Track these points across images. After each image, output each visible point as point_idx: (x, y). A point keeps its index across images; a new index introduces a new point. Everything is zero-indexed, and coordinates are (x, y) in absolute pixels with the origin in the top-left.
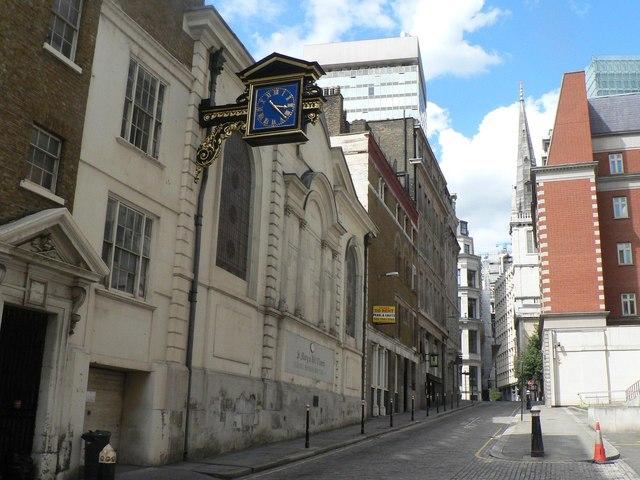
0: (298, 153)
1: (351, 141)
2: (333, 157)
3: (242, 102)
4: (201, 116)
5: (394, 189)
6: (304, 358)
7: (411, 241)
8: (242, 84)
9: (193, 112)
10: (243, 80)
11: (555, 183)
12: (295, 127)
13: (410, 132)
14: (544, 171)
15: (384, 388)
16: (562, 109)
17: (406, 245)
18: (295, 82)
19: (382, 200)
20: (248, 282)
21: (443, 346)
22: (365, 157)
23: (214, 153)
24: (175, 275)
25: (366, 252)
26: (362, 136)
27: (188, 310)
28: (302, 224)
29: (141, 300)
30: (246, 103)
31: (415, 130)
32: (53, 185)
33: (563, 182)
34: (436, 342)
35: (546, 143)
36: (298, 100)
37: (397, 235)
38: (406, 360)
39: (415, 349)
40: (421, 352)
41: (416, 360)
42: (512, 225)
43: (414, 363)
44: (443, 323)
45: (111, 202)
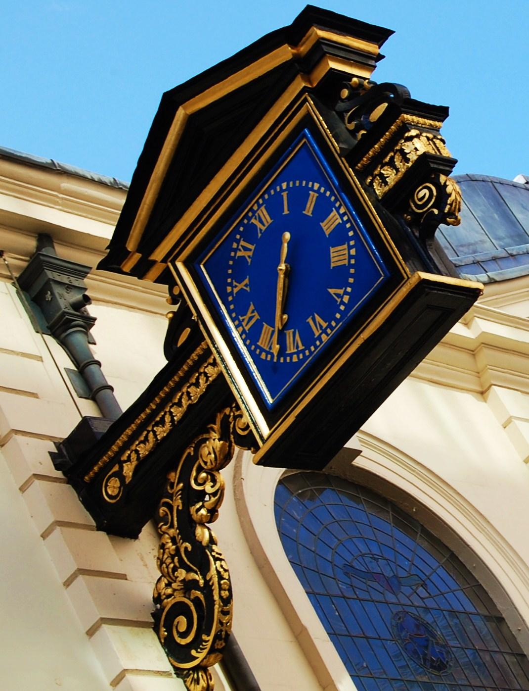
0: (482, 371)
3: (184, 344)
4: (90, 498)
8: (148, 282)
9: (58, 499)
10: (140, 271)
16: (160, 633)
18: (297, 133)
23: (207, 589)
32: (310, 485)
36: (346, 187)
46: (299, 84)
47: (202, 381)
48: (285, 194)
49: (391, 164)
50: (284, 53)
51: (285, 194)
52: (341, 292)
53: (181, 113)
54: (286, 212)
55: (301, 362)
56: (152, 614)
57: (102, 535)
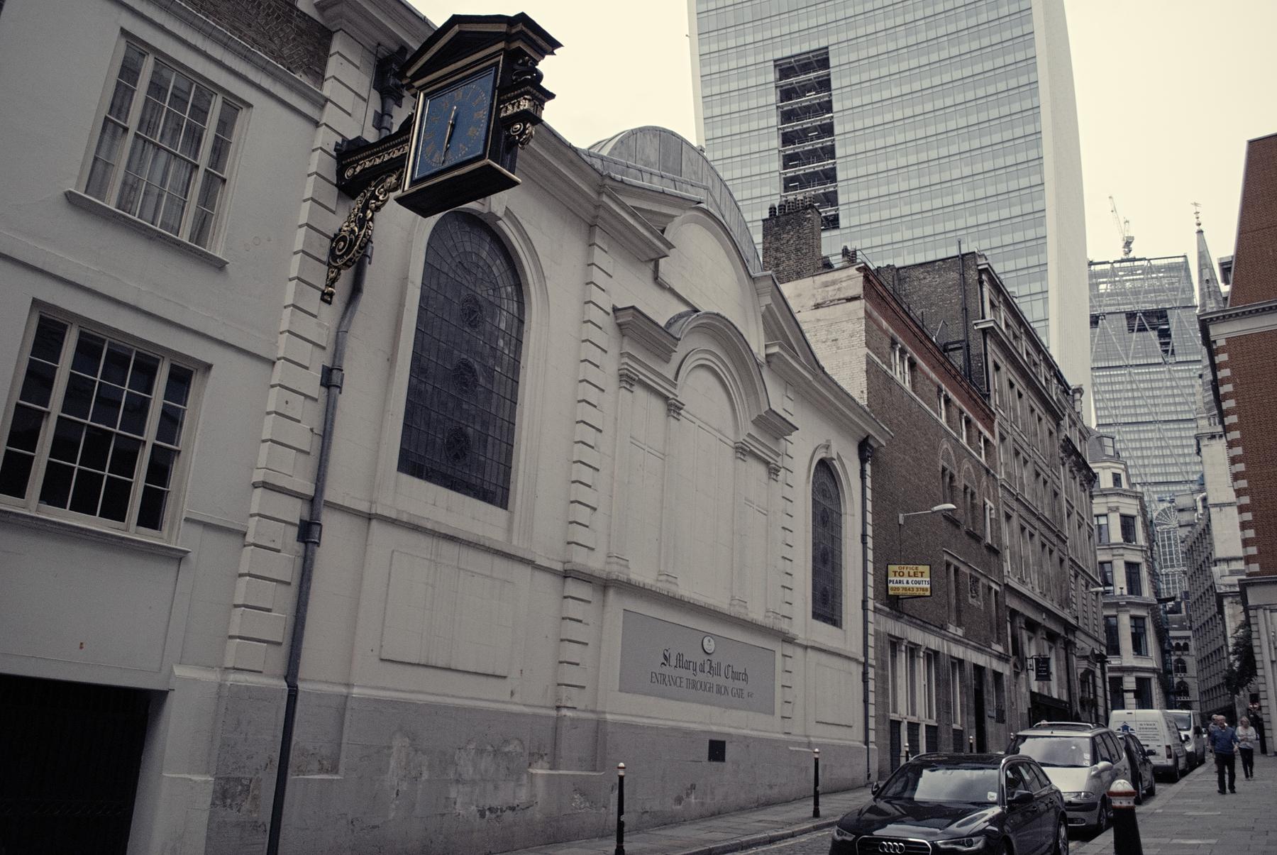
1: (834, 282)
4: (340, 173)
5: (933, 368)
6: (682, 663)
7: (983, 460)
11: (1248, 338)
13: (972, 276)
14: (1225, 318)
15: (924, 717)
17: (966, 465)
19: (907, 386)
21: (1069, 645)
22: (859, 307)
23: (357, 237)
24: (255, 486)
25: (863, 472)
27: (299, 561)
28: (674, 409)
29: (147, 536)
31: (981, 272)
33: (1263, 334)
37: (946, 445)
38: (979, 670)
39: (1000, 649)
41: (1006, 669)
42: (1198, 438)
43: (998, 676)
44: (1066, 602)
45: (49, 331)
46: (501, 45)
50: (503, 28)
53: (456, 28)
56: (551, 45)
57: (336, 189)
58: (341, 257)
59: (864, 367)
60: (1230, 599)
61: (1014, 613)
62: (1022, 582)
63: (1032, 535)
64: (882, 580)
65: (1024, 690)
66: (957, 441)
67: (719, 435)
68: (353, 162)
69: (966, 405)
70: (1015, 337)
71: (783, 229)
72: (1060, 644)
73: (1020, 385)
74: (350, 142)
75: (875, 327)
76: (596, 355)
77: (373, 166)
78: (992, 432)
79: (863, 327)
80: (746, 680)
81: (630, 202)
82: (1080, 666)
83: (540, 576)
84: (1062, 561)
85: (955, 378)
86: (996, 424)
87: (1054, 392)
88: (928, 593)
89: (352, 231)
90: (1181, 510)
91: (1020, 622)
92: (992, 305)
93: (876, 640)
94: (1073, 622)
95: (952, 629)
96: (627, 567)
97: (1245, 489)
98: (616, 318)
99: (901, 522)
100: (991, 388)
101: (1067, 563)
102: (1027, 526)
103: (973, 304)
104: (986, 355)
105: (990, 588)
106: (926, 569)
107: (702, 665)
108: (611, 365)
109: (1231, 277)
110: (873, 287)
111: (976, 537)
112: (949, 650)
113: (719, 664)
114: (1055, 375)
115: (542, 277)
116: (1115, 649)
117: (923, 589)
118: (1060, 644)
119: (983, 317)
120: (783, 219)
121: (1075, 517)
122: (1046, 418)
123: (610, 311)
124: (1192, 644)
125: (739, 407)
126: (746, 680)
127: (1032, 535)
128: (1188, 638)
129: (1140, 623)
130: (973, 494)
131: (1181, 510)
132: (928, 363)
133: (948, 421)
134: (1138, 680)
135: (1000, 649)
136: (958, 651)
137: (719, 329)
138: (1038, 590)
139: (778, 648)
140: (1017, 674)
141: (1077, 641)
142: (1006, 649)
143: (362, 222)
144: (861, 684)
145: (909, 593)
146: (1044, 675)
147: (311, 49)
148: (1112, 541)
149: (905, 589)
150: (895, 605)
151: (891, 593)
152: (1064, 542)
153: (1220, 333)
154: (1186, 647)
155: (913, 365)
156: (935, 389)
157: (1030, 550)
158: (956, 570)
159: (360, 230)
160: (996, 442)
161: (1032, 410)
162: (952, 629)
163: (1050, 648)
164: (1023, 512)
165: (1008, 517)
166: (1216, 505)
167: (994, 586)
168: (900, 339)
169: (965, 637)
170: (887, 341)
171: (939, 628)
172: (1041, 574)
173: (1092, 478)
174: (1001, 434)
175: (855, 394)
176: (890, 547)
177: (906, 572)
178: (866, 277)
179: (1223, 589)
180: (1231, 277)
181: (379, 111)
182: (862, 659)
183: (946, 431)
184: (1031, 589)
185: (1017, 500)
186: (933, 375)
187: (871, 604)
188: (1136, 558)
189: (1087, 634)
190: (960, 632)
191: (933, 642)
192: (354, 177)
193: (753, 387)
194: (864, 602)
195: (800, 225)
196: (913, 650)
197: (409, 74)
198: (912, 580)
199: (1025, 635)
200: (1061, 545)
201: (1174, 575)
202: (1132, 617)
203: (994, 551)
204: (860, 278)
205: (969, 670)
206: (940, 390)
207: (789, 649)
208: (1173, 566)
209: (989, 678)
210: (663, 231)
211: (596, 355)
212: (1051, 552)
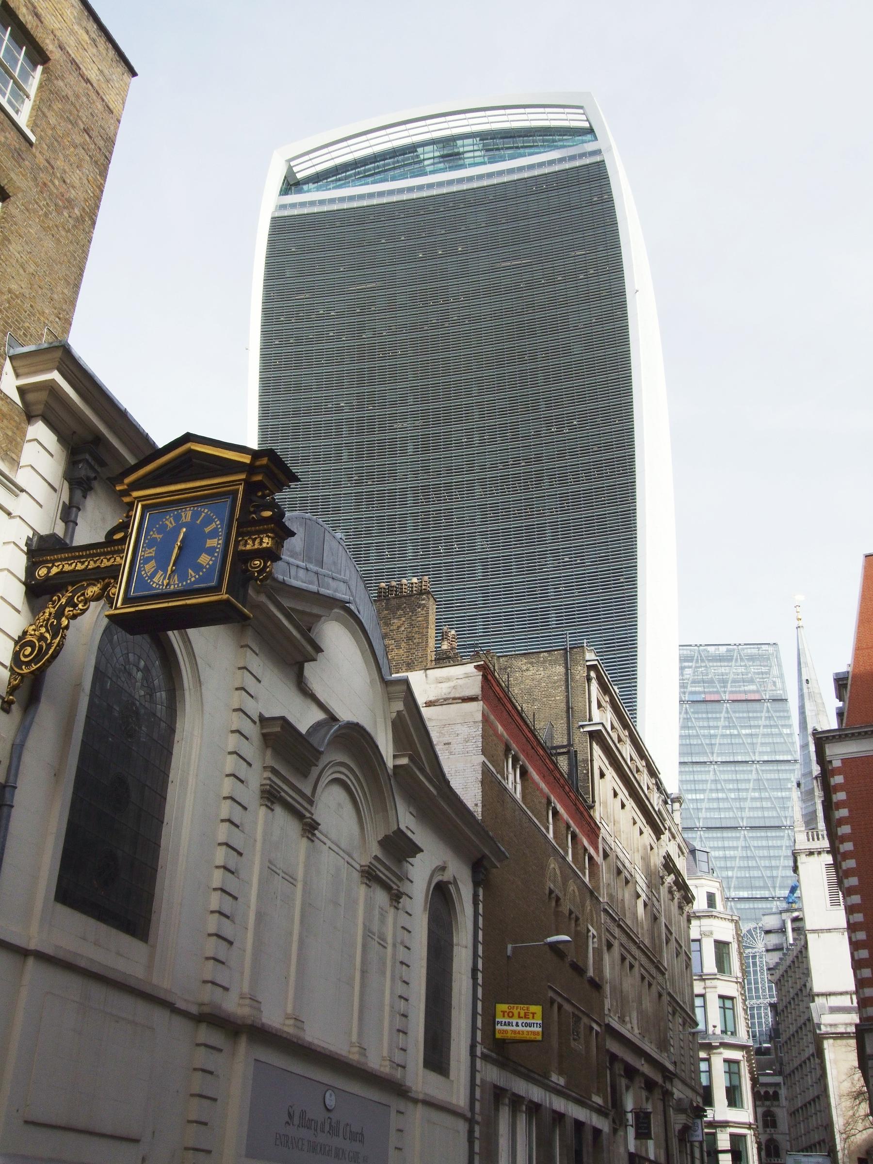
2: (390, 698)
4: (30, 570)
5: (543, 777)
6: (306, 1123)
12: (217, 589)
17: (572, 887)
20: (154, 947)
21: (667, 1094)
22: (476, 709)
23: (49, 646)
26: (470, 668)
28: (310, 828)
30: (123, 541)
31: (590, 668)
34: (650, 1085)
35: (841, 683)
38: (579, 1125)
39: (598, 1100)
40: (613, 1110)
43: (597, 1132)
44: (663, 1045)
47: (112, 560)
48: (203, 514)
49: (254, 540)
51: (203, 514)
52: (193, 574)
54: (198, 522)
55: (155, 589)
58: (28, 664)
59: (480, 777)
60: (831, 1041)
61: (613, 1057)
62: (622, 1020)
63: (632, 967)
64: (490, 1021)
65: (622, 1150)
66: (564, 859)
67: (346, 857)
68: (47, 562)
69: (572, 818)
70: (620, 740)
71: (394, 613)
72: (657, 1094)
73: (623, 794)
74: (41, 538)
75: (491, 732)
76: (243, 770)
77: (74, 571)
78: (596, 849)
79: (480, 732)
80: (362, 1141)
81: (287, 603)
82: (678, 1121)
83: (177, 1021)
84: (660, 995)
85: (563, 787)
86: (600, 839)
87: (656, 800)
88: (539, 1038)
89: (42, 638)
90: (768, 932)
91: (619, 1068)
92: (600, 706)
93: (482, 1092)
94: (671, 1067)
95: (554, 1078)
96: (259, 1010)
97: (860, 923)
98: (262, 727)
99: (509, 953)
100: (597, 799)
101: (666, 998)
102: (628, 956)
103: (578, 703)
104: (592, 760)
105: (592, 1028)
106: (537, 1009)
107: (323, 1124)
108: (256, 778)
109: (847, 696)
110: (491, 687)
111: (579, 969)
112: (551, 1103)
113: (338, 1122)
114: (657, 784)
115: (199, 682)
116: (708, 1099)
117: (534, 1033)
118: (657, 1094)
119: (590, 720)
120: (394, 602)
121: (673, 944)
122: (648, 830)
123: (257, 719)
124: (783, 1092)
125: (368, 826)
126: (362, 1141)
127: (632, 967)
128: (777, 1085)
129: (734, 1067)
130: (577, 919)
131: (768, 932)
132: (539, 773)
133: (555, 837)
134: (733, 1136)
135: (598, 1100)
136: (560, 1104)
137: (355, 739)
138: (636, 1031)
139: (396, 1104)
140: (615, 1131)
141: (675, 1090)
142: (605, 1101)
143: (56, 630)
144: (466, 1144)
145: (518, 1037)
146: (643, 1133)
147: (10, 433)
148: (705, 971)
149: (514, 1032)
150: (501, 1051)
151: (498, 1036)
152: (663, 974)
153: (837, 752)
154: (776, 1096)
155: (524, 773)
156: (544, 801)
157: (630, 984)
158: (560, 1007)
159: (54, 637)
160: (599, 859)
161: (635, 823)
162: (554, 1078)
163: (647, 1099)
164: (624, 940)
165: (610, 946)
166: (814, 931)
167: (595, 1026)
168: (514, 746)
169: (566, 1087)
170: (501, 748)
171: (540, 1079)
172: (641, 1012)
173: (688, 898)
174: (604, 851)
175: (470, 804)
176: (500, 983)
177: (516, 1012)
178: (484, 677)
179: (824, 1029)
180: (847, 696)
181: (67, 502)
182: (469, 1115)
183: (554, 848)
184: (631, 1029)
185: (619, 926)
186: (543, 785)
187: (479, 1050)
188: (731, 989)
189: (684, 1082)
190: (562, 1081)
191: (536, 1094)
192: (47, 578)
193: (382, 804)
194: (473, 1047)
195: (413, 611)
196: (516, 1101)
197: (127, 480)
198: (522, 1022)
199: (624, 1082)
200: (660, 978)
201: (759, 1008)
202: (725, 1061)
203: (596, 985)
204: (478, 677)
205: (570, 1127)
206: (549, 802)
207: (402, 1105)
208: (758, 998)
209: (588, 1136)
210: (309, 630)
211: (243, 770)
212: (650, 985)
